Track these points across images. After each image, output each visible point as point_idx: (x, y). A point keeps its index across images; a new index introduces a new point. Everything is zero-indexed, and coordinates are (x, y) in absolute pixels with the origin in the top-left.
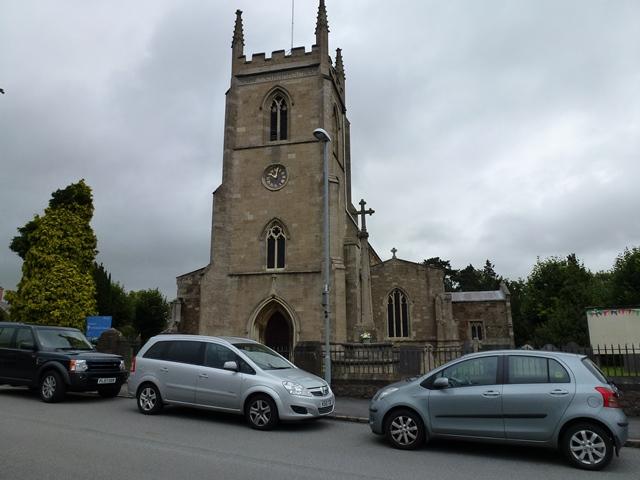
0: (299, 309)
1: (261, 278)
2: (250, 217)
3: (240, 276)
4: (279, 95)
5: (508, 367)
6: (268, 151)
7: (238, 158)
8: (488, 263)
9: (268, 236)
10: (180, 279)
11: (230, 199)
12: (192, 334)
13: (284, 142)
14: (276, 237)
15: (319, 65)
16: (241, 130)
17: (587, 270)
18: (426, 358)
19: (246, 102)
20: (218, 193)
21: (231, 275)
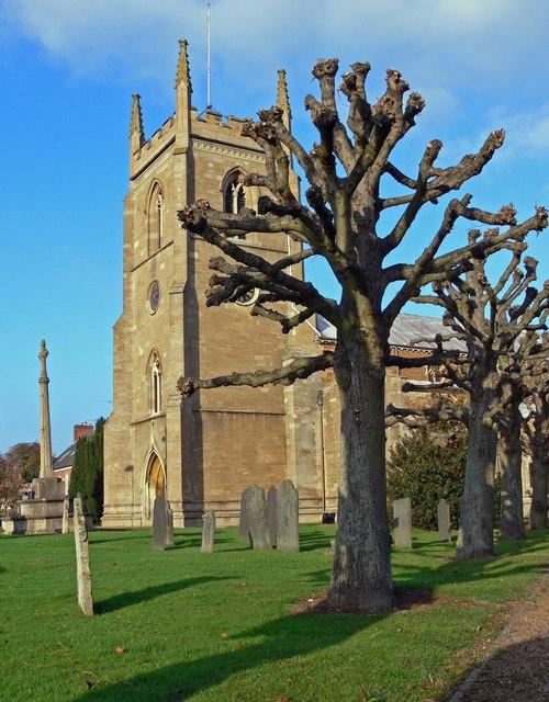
11: (129, 334)
21: (131, 425)
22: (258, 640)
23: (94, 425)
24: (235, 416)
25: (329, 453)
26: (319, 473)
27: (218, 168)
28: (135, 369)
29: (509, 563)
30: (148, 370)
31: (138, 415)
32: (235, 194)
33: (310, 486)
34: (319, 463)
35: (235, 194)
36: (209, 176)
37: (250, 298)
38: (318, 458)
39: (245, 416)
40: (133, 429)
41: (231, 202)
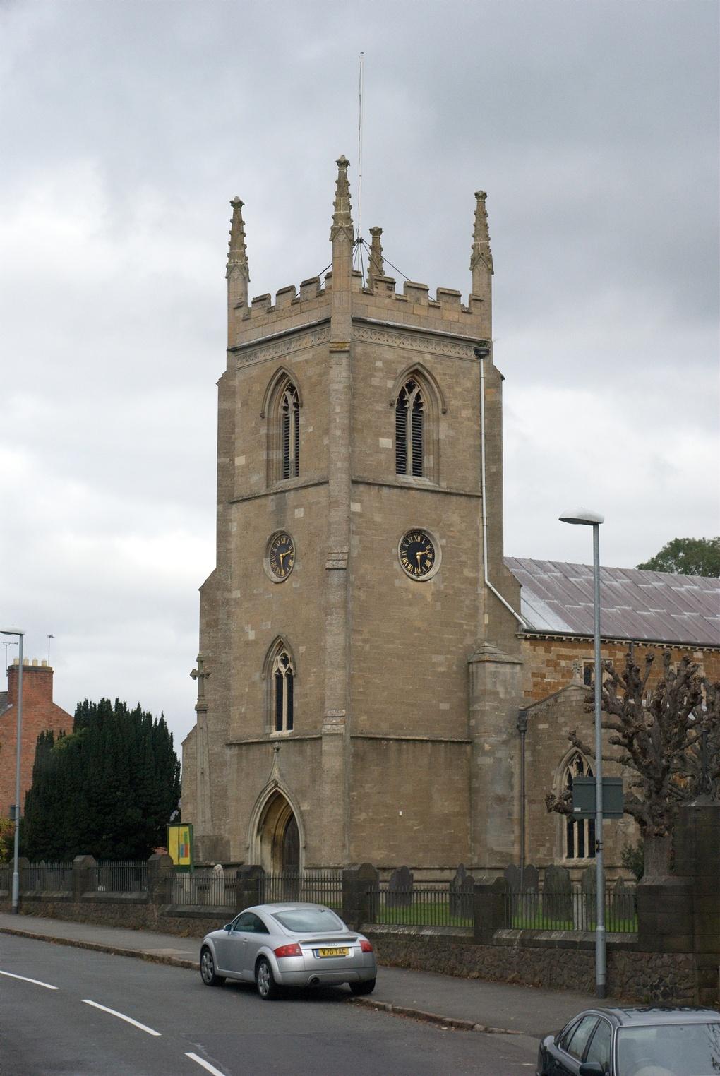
0: (305, 807)
1: (264, 748)
2: (252, 635)
3: (240, 745)
4: (284, 383)
5: (277, 904)
6: (270, 503)
7: (236, 512)
8: (139, 706)
9: (275, 670)
10: (182, 744)
11: (227, 601)
12: (14, 841)
13: (292, 482)
14: (283, 670)
15: (328, 321)
16: (240, 461)
17: (131, 708)
18: (575, 899)
19: (245, 404)
20: (208, 591)
21: (230, 745)
22: (568, 1042)
23: (640, 837)
24: (404, 745)
25: (532, 802)
26: (517, 829)
27: (389, 370)
28: (236, 659)
29: (314, 936)
30: (267, 665)
31: (238, 731)
32: (410, 405)
33: (504, 850)
34: (516, 816)
35: (410, 405)
36: (375, 382)
37: (428, 569)
38: (516, 808)
39: (418, 745)
40: (230, 753)
41: (404, 420)
